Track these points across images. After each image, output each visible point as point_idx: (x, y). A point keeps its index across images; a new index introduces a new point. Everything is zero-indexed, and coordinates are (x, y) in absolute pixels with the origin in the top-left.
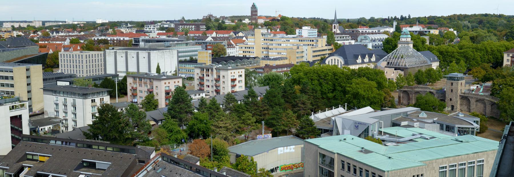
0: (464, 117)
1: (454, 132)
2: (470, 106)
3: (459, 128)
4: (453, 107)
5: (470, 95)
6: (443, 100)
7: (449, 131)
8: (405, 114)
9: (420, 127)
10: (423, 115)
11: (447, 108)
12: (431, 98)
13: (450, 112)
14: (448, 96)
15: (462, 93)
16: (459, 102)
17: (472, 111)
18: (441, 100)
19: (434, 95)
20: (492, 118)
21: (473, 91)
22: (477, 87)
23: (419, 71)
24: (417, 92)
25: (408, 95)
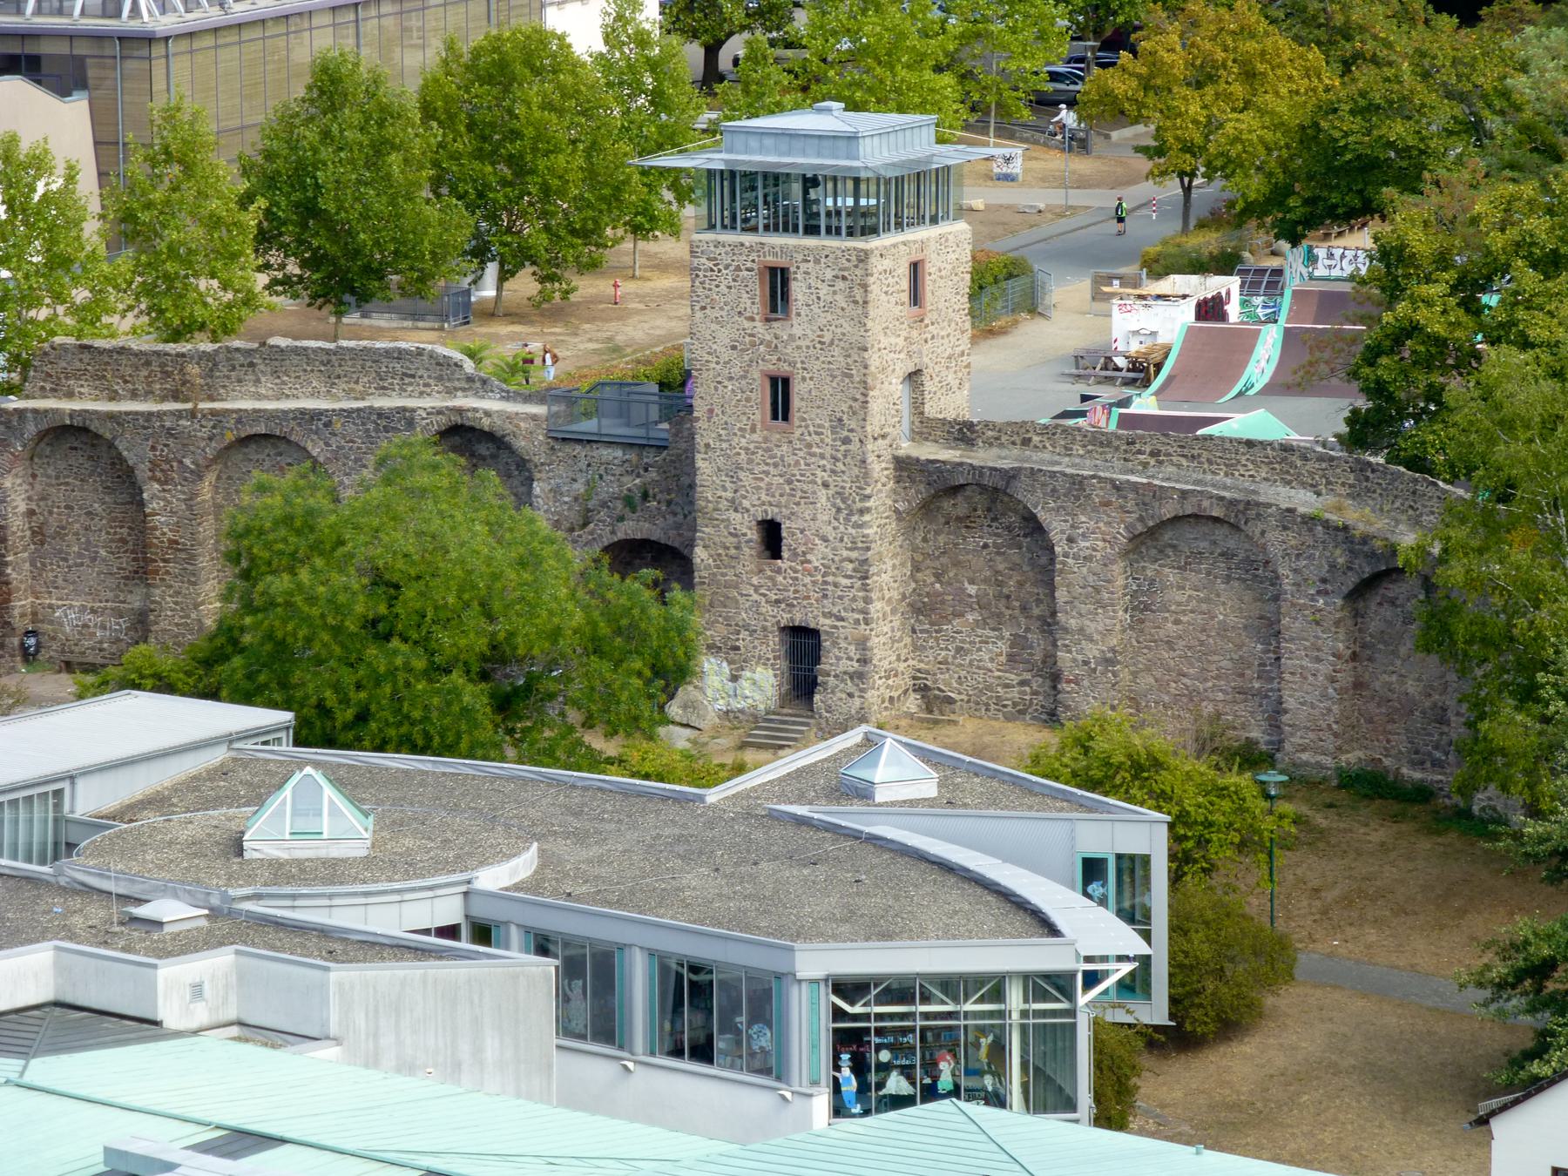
0: (949, 801)
1: (770, 1067)
2: (1049, 624)
3: (850, 988)
4: (803, 645)
5: (1042, 458)
6: (667, 559)
7: (703, 1052)
8: (36, 826)
9: (249, 1030)
10: (316, 812)
11: (713, 670)
12: (465, 527)
13: (763, 734)
14: (735, 468)
15: (925, 428)
16: (889, 576)
17: (1087, 701)
18: (628, 555)
19: (519, 471)
20: (1369, 787)
21: (1141, 372)
22: (1211, 309)
23: (329, 86)
24: (265, 440)
25: (125, 481)
